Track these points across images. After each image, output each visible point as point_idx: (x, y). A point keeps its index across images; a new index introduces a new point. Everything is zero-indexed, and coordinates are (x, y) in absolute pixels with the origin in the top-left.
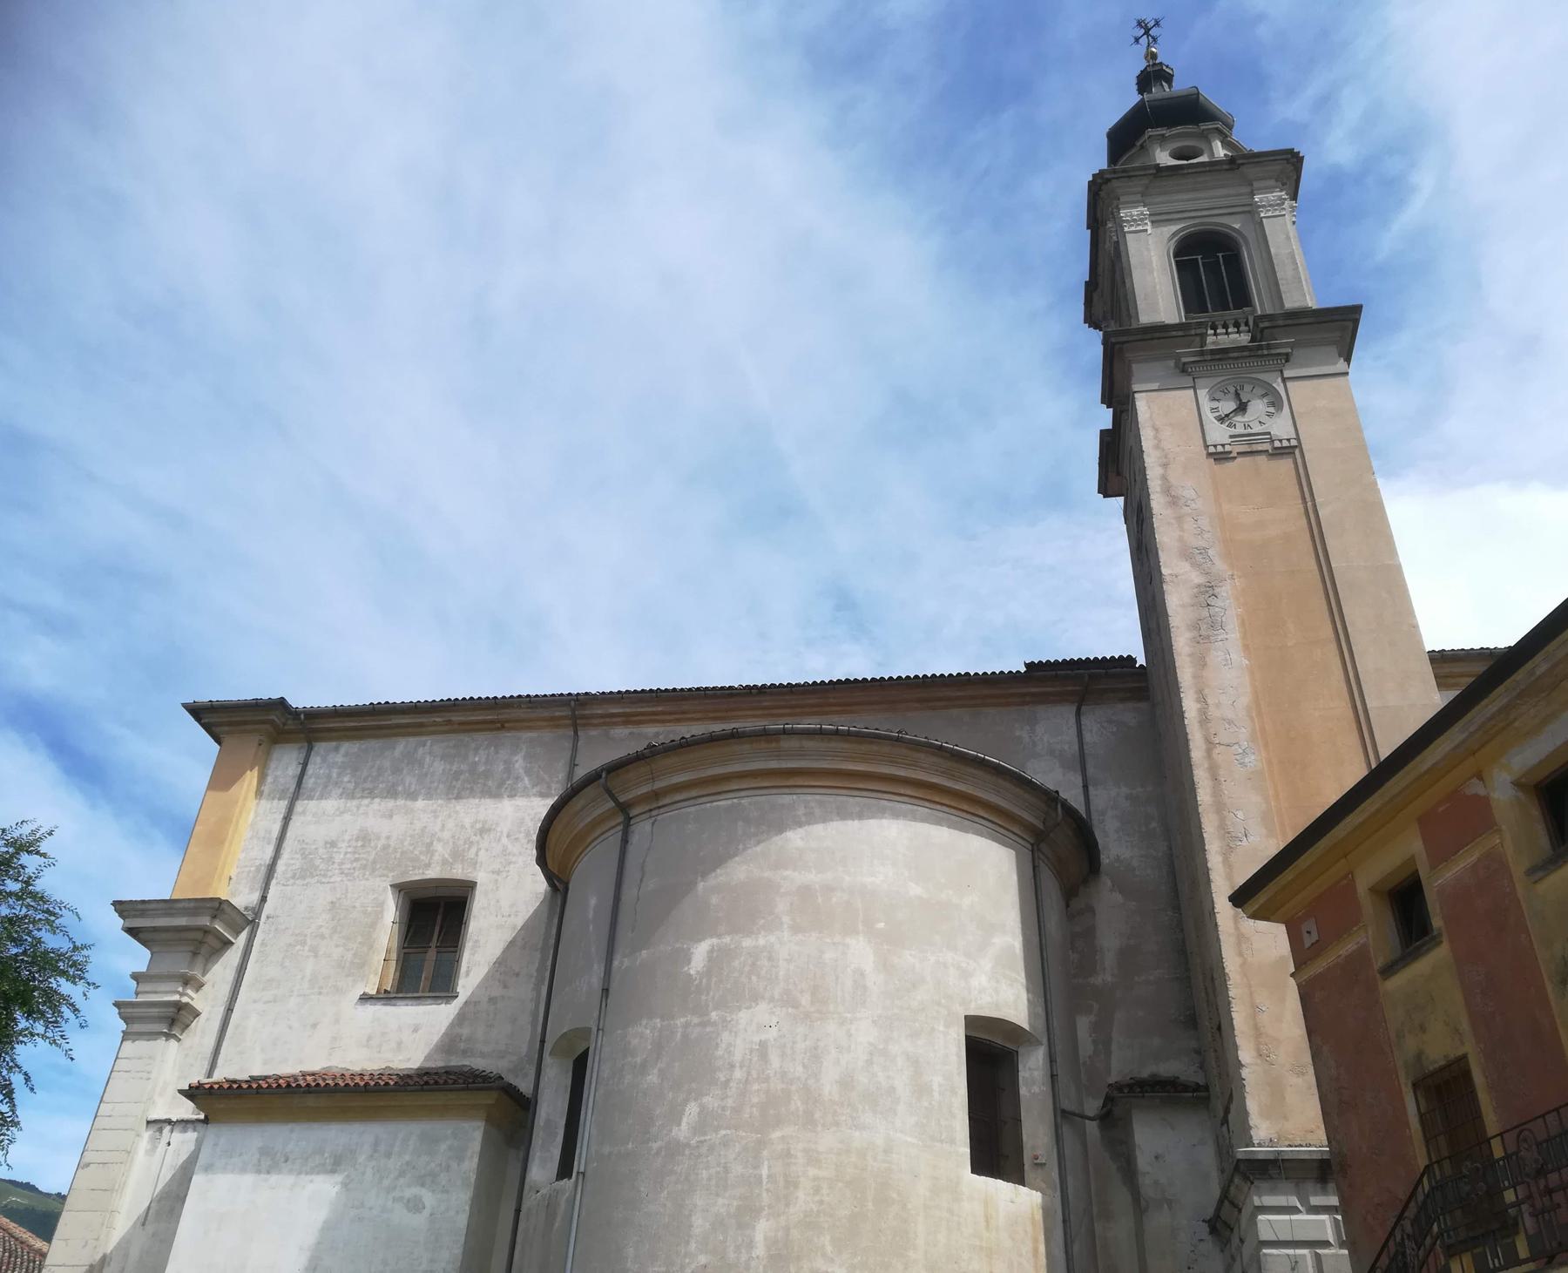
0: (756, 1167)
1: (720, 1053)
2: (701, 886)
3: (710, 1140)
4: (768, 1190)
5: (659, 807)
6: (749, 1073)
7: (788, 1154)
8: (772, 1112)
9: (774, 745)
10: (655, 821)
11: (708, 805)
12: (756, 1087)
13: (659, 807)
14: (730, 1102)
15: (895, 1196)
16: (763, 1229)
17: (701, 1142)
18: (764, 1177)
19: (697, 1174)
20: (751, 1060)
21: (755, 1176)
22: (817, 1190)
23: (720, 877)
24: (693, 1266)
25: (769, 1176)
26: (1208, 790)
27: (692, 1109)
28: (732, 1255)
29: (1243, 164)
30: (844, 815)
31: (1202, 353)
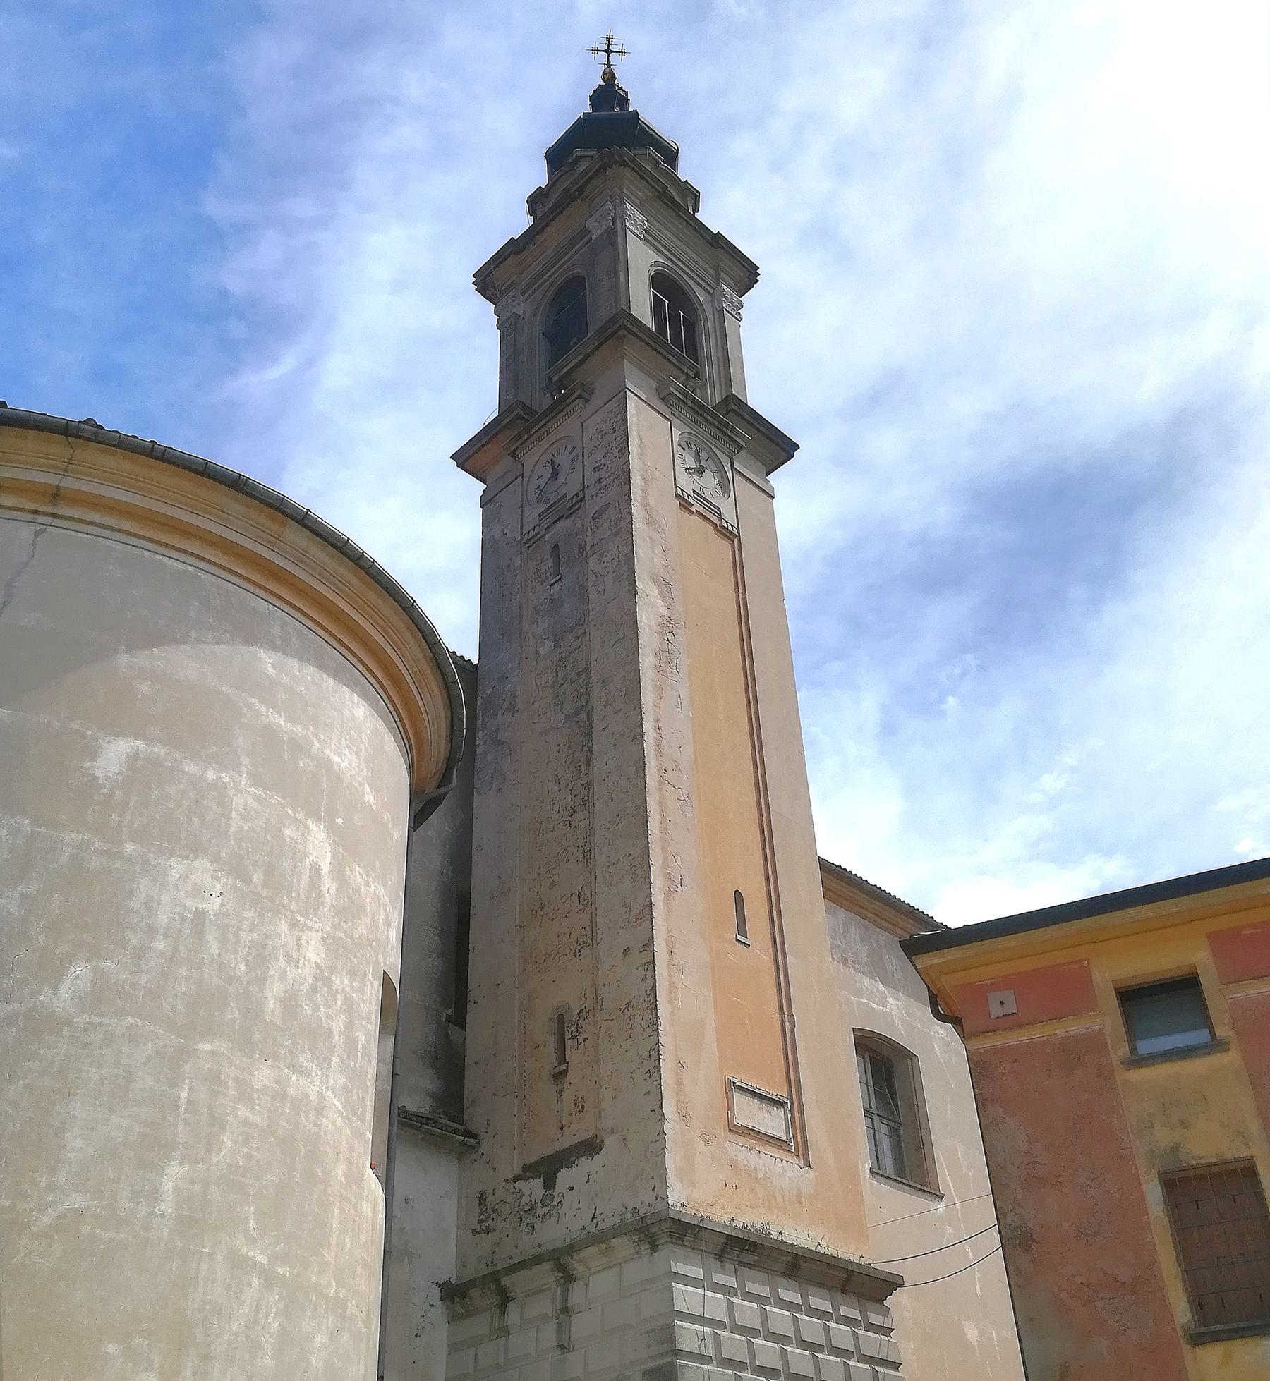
0: (174, 1084)
1: (134, 904)
2: (123, 659)
3: (108, 1025)
4: (186, 1121)
5: (54, 516)
6: (176, 949)
7: (215, 1079)
8: (202, 1013)
9: (276, 527)
10: (42, 531)
11: (146, 554)
12: (184, 971)
13: (54, 516)
14: (144, 980)
15: (319, 1172)
16: (173, 1176)
17: (95, 1025)
18: (183, 1101)
19: (80, 1071)
20: (180, 931)
21: (170, 1097)
22: (247, 1139)
23: (157, 658)
24: (62, 1208)
25: (190, 1102)
26: (657, 823)
27: (79, 975)
28: (125, 1205)
29: (723, 248)
30: (322, 666)
31: (686, 394)
